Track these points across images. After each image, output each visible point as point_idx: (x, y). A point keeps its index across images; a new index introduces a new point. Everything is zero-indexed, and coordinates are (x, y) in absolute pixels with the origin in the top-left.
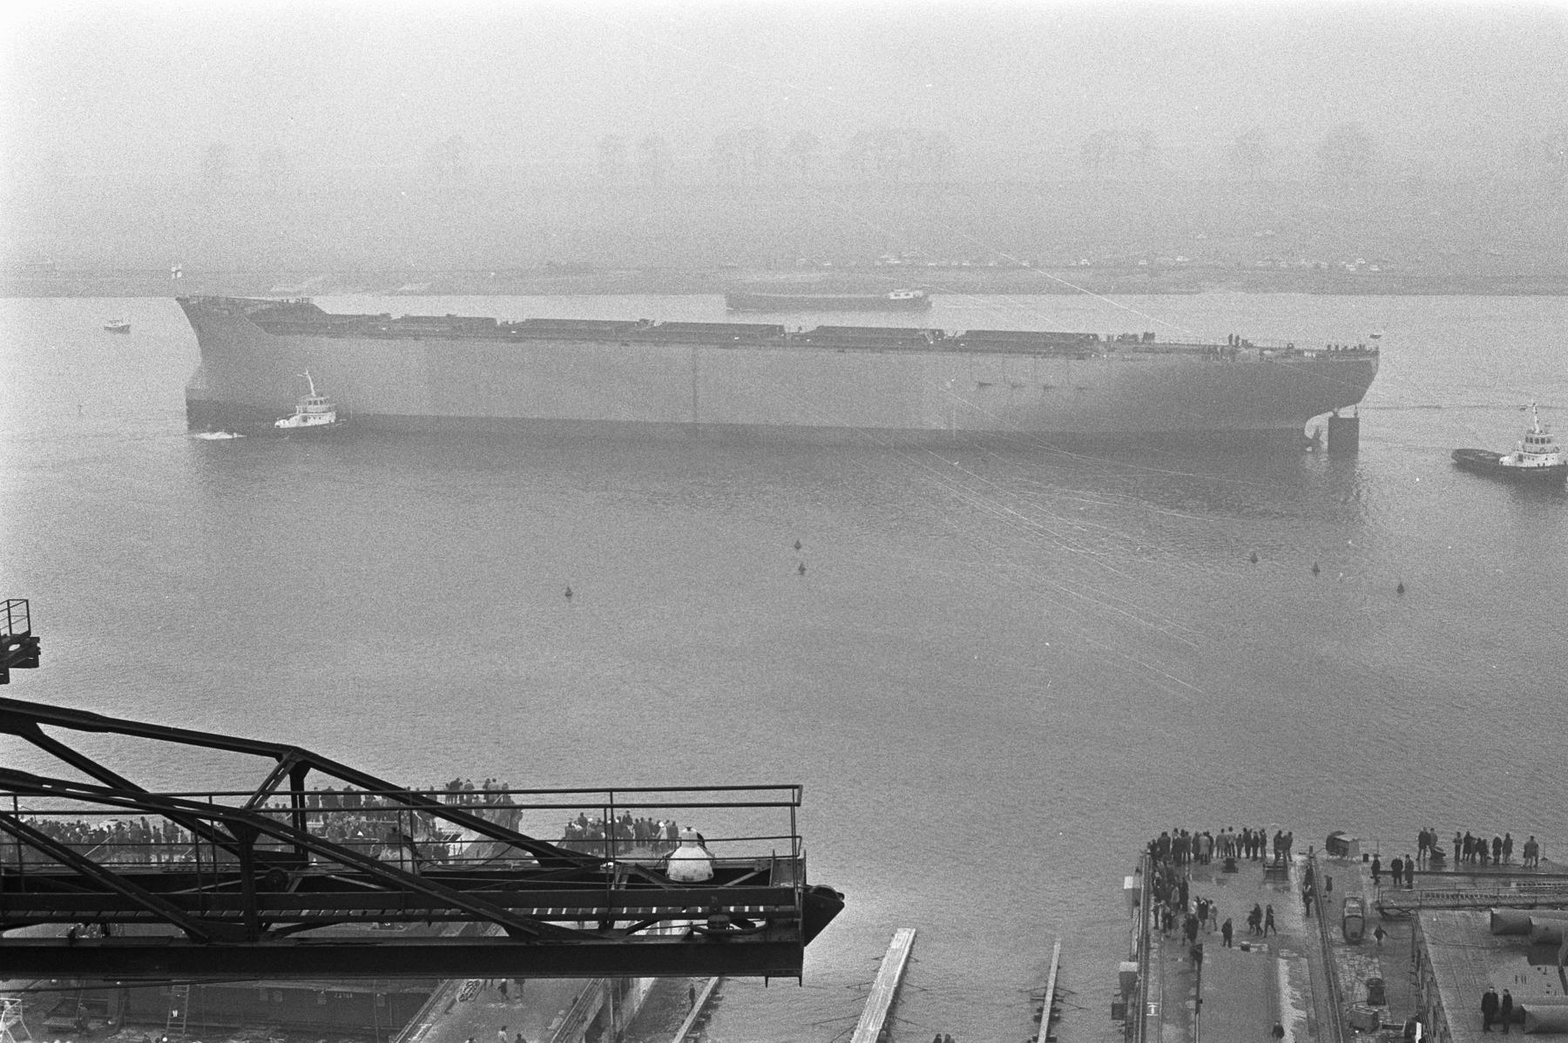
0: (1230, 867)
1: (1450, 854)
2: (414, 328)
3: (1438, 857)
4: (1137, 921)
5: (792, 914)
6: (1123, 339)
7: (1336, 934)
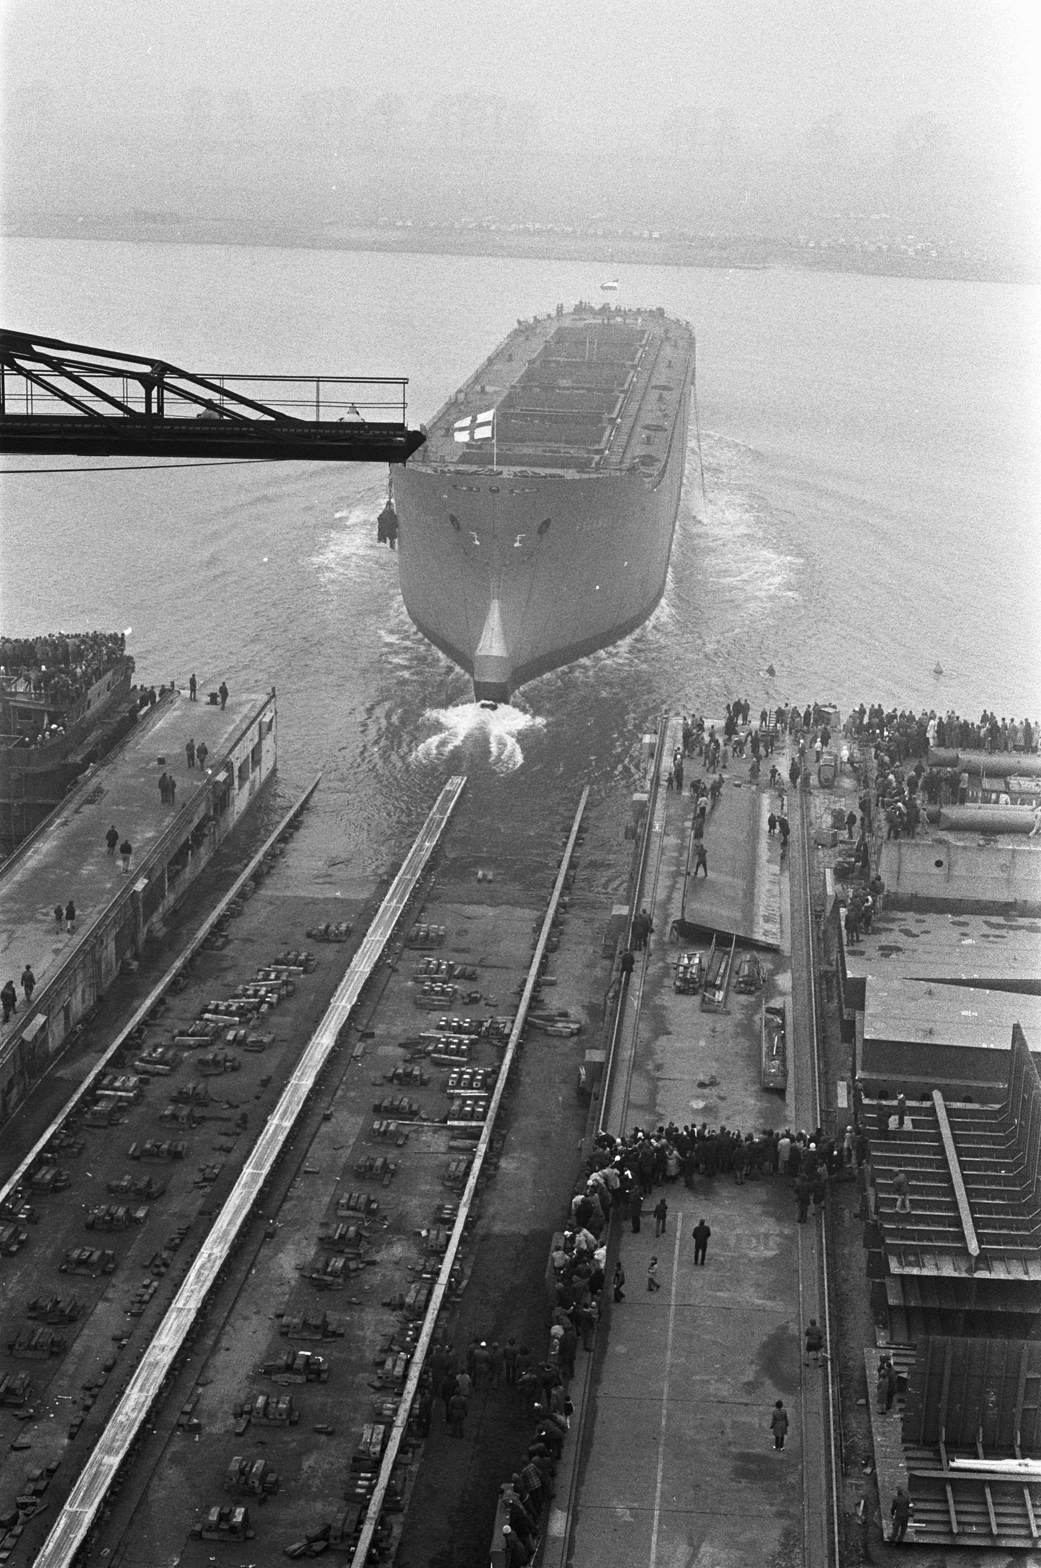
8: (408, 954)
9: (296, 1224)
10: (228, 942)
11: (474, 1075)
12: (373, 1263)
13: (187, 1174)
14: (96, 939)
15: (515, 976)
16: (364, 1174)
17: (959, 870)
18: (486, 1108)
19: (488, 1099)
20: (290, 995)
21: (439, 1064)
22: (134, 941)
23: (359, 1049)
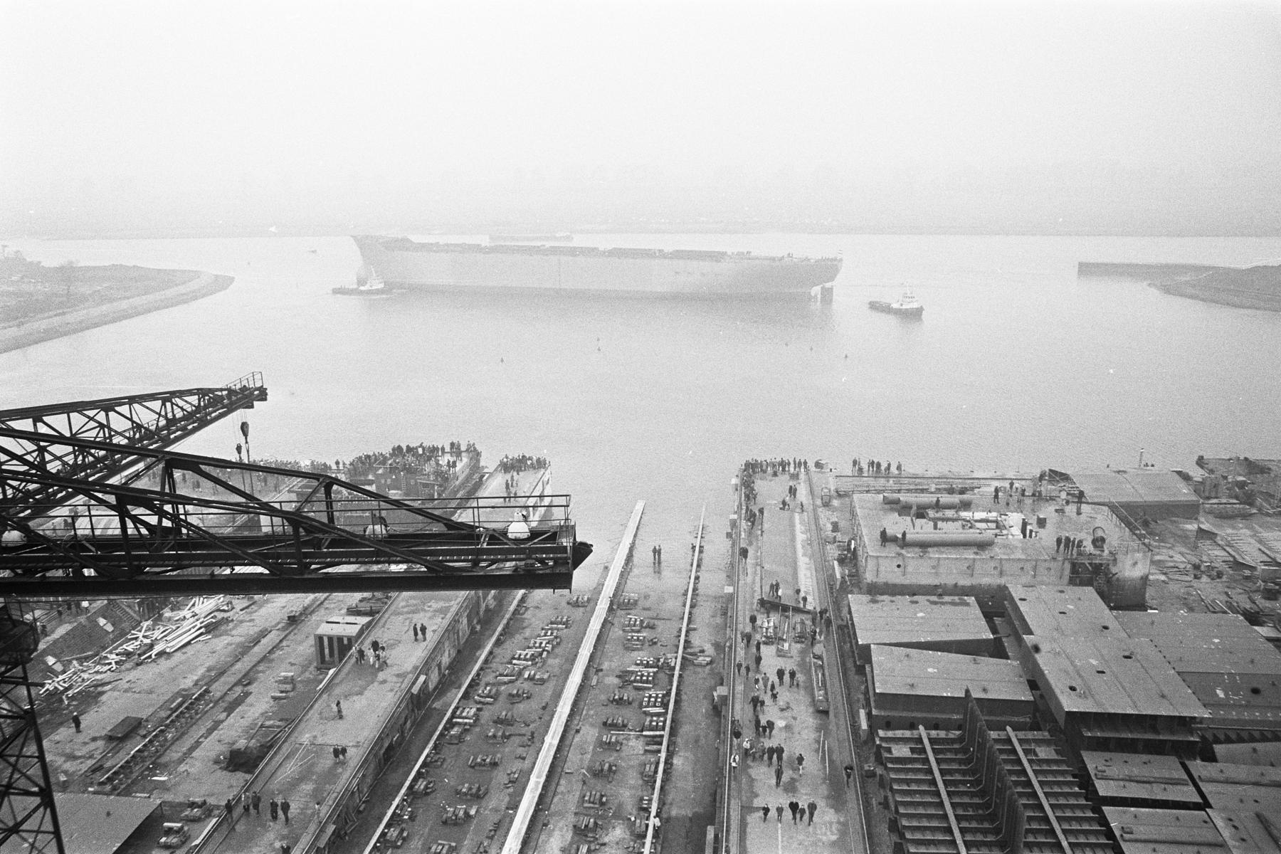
0: (775, 474)
1: (865, 467)
2: (447, 248)
3: (861, 470)
4: (736, 497)
5: (566, 558)
6: (738, 254)
7: (819, 502)
8: (620, 612)
9: (561, 814)
10: (527, 609)
11: (657, 697)
12: (604, 844)
13: (500, 777)
14: (455, 621)
15: (676, 625)
16: (598, 774)
17: (910, 569)
18: (664, 722)
19: (666, 713)
20: (558, 644)
21: (637, 689)
22: (478, 613)
23: (594, 682)
